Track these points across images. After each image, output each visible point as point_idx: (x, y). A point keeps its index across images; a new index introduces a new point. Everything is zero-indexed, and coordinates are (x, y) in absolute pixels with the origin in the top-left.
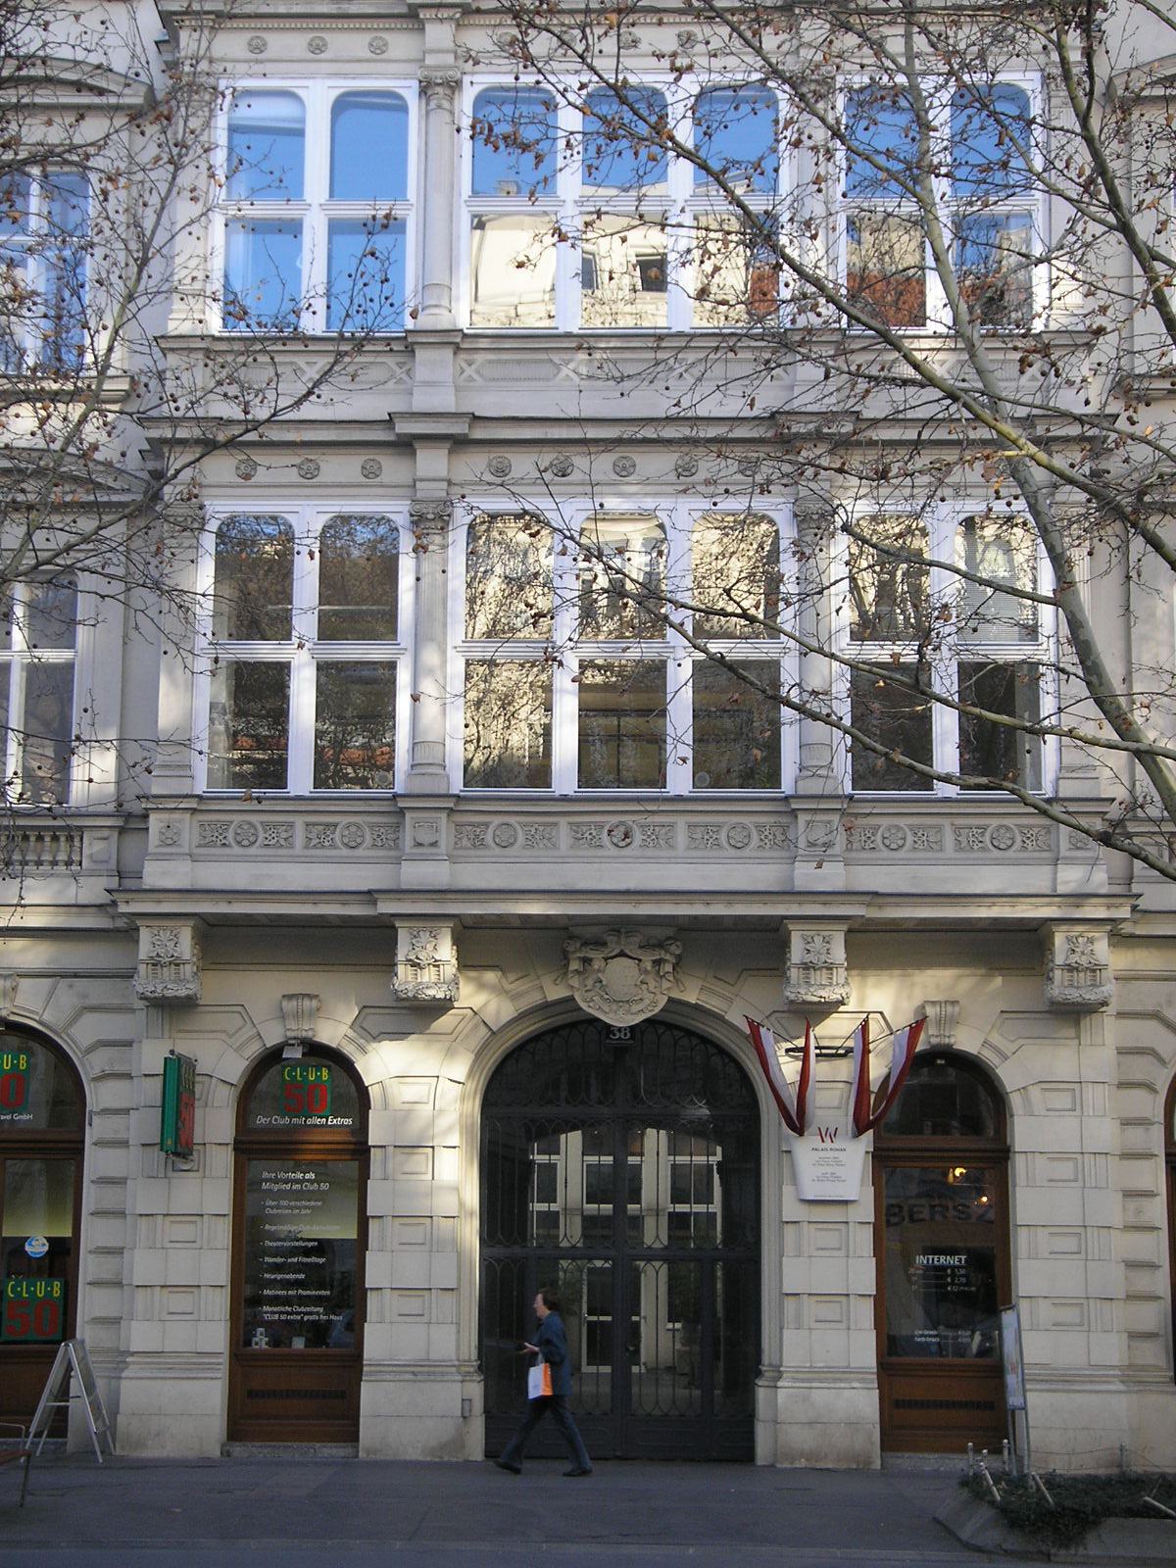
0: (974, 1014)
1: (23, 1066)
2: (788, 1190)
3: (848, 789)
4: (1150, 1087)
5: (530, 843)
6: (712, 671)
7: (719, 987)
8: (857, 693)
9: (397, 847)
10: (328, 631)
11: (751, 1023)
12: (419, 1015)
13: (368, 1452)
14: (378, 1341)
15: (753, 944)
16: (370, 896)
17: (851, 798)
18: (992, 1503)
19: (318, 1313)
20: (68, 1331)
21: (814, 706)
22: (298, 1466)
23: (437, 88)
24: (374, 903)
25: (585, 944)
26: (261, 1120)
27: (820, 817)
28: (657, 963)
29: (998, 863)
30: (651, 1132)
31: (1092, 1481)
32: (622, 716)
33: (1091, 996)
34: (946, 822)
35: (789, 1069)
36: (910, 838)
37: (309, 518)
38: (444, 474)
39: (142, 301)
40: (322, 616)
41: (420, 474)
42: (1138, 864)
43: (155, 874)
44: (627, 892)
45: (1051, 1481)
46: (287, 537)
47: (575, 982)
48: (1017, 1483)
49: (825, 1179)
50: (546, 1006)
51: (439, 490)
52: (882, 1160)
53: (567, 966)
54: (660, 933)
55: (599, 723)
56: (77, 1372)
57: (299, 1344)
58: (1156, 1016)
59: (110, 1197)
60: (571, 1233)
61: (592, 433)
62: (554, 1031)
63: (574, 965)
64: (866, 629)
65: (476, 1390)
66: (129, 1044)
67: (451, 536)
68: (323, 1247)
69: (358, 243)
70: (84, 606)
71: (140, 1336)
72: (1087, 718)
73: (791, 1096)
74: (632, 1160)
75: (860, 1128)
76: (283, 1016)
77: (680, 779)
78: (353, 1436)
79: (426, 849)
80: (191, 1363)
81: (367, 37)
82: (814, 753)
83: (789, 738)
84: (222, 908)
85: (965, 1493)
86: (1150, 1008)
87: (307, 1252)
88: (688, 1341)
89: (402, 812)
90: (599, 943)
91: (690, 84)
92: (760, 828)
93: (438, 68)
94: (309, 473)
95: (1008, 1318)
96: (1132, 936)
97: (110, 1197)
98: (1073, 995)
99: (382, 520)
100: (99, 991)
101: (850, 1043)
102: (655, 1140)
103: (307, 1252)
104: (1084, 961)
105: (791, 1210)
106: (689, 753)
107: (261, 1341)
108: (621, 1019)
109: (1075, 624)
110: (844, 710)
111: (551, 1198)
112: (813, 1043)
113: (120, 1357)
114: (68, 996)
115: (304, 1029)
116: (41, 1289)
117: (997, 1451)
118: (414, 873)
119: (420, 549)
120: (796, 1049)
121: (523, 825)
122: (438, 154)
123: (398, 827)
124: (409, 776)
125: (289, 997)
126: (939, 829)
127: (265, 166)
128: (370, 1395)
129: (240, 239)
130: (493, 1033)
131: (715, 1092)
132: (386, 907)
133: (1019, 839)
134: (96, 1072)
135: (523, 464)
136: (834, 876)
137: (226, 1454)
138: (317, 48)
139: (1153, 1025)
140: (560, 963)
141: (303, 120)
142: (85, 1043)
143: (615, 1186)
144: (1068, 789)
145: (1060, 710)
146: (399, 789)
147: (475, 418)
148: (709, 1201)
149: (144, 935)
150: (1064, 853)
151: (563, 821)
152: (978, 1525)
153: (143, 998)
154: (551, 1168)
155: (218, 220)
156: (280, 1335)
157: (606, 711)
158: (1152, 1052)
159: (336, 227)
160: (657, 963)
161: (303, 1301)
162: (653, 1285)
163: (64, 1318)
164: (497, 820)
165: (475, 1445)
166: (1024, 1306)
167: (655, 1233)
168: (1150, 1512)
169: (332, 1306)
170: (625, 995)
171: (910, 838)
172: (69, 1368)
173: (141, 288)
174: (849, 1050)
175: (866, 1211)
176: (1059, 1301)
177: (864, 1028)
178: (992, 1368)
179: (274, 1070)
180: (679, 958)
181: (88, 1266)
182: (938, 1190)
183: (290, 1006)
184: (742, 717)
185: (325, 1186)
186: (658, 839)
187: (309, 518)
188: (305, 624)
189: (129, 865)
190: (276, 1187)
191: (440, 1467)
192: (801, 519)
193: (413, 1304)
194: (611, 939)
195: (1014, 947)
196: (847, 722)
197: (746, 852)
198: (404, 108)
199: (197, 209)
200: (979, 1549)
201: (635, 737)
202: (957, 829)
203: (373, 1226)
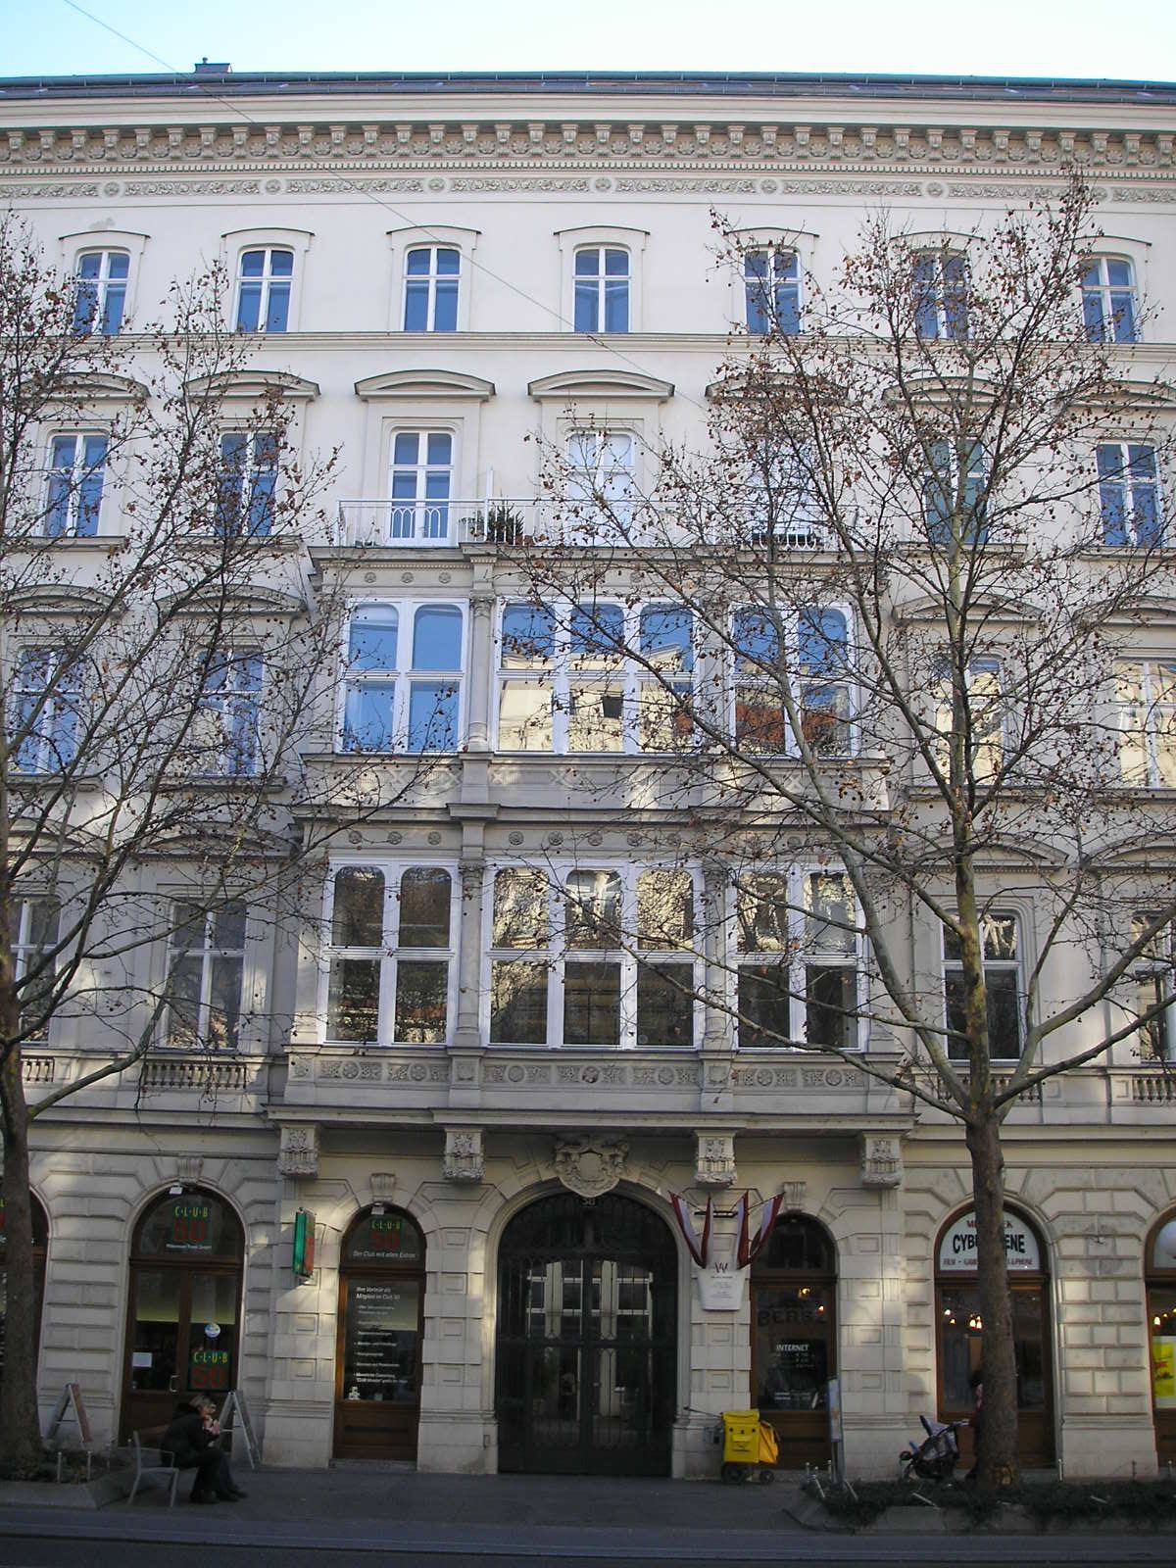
0: (815, 1191)
1: (205, 1215)
2: (695, 1304)
3: (736, 1047)
4: (926, 1237)
5: (531, 1080)
6: (649, 973)
7: (654, 1173)
8: (742, 990)
9: (447, 1080)
10: (405, 940)
11: (672, 1196)
12: (464, 1187)
13: (423, 1466)
14: (428, 1397)
15: (674, 1145)
16: (429, 1112)
17: (737, 1052)
18: (820, 1499)
19: (389, 1379)
20: (231, 1384)
21: (715, 1000)
22: (379, 1475)
23: (480, 604)
24: (432, 1116)
25: (567, 1144)
26: (357, 1254)
27: (717, 1064)
28: (613, 1157)
29: (829, 1094)
30: (607, 1264)
31: (883, 1484)
32: (592, 992)
33: (888, 1179)
34: (798, 1068)
35: (696, 1225)
36: (775, 1078)
37: (393, 870)
38: (480, 842)
39: (296, 736)
40: (401, 932)
41: (465, 842)
42: (918, 1099)
43: (291, 1094)
44: (595, 1111)
45: (858, 1486)
46: (380, 876)
47: (560, 1168)
48: (836, 1488)
49: (720, 1295)
50: (540, 1184)
51: (477, 852)
52: (755, 1284)
53: (554, 1158)
54: (614, 1137)
55: (573, 997)
56: (238, 1411)
57: (378, 1398)
58: (929, 1191)
59: (260, 1301)
60: (552, 1329)
61: (574, 818)
62: (546, 1199)
63: (559, 1158)
64: (748, 944)
65: (492, 1430)
66: (273, 1203)
67: (484, 890)
68: (394, 1336)
69: (430, 697)
70: (251, 927)
71: (278, 1390)
72: (886, 1005)
73: (698, 1243)
74: (595, 1280)
75: (741, 1266)
76: (371, 1187)
77: (628, 1042)
78: (414, 1457)
79: (465, 1082)
80: (310, 1408)
81: (438, 573)
82: (715, 1025)
83: (699, 1019)
84: (334, 1117)
85: (804, 1494)
86: (925, 1185)
87: (385, 1339)
88: (629, 1399)
89: (450, 1058)
90: (577, 1144)
91: (638, 608)
92: (680, 1071)
93: (482, 591)
94: (394, 840)
95: (833, 1384)
96: (915, 1140)
97: (260, 1301)
98: (877, 1178)
99: (441, 871)
100: (256, 1169)
101: (736, 1209)
102: (608, 1268)
103: (385, 1339)
104: (884, 1156)
105: (697, 1316)
106: (634, 1030)
107: (354, 1395)
108: (589, 1192)
109: (877, 946)
110: (733, 1002)
111: (539, 1303)
112: (712, 1209)
113: (265, 1403)
114: (235, 1170)
115: (387, 1196)
116: (215, 1357)
117: (823, 1467)
118: (457, 1098)
119: (467, 896)
120: (702, 1213)
121: (528, 1067)
122: (479, 638)
123: (448, 1067)
124: (455, 1035)
125: (377, 1175)
126: (794, 1072)
127: (376, 655)
128: (425, 1432)
129: (355, 693)
130: (507, 1201)
131: (649, 1241)
132: (439, 1119)
133: (844, 1078)
134: (252, 1220)
135: (534, 838)
136: (728, 1102)
137: (332, 1465)
138: (407, 579)
139: (928, 1197)
140: (551, 1156)
141: (397, 622)
142: (245, 1200)
143: (584, 1296)
144: (875, 1047)
145: (868, 1001)
146: (448, 1042)
147: (502, 807)
148: (645, 1308)
149: (285, 1134)
150: (872, 1087)
151: (553, 1065)
152: (810, 1513)
153: (283, 1174)
154: (540, 1286)
155: (342, 685)
156: (366, 1391)
157: (580, 991)
158: (926, 1214)
159: (415, 687)
160: (613, 1157)
161: (382, 1370)
162: (608, 1361)
163: (229, 1375)
164: (512, 1064)
165: (492, 1467)
166: (844, 1377)
167: (608, 1330)
168: (915, 1502)
169: (399, 1373)
170: (592, 1178)
171: (775, 1078)
172: (233, 1408)
173: (296, 728)
174: (736, 1214)
175: (745, 1316)
176: (866, 1374)
177: (745, 1199)
178: (823, 1415)
179: (365, 1224)
180: (627, 1154)
181: (245, 1344)
182: (791, 1302)
183: (376, 1181)
184: (669, 1002)
185: (397, 1297)
186: (614, 1077)
187: (393, 870)
188: (391, 940)
189: (275, 1088)
190: (365, 1297)
191: (469, 1478)
192: (707, 874)
193: (453, 1375)
194: (584, 1141)
195: (839, 1146)
196: (735, 1009)
197: (670, 1086)
198: (460, 615)
199: (331, 681)
200: (811, 1528)
201: (600, 1008)
202: (805, 1072)
203: (428, 1324)
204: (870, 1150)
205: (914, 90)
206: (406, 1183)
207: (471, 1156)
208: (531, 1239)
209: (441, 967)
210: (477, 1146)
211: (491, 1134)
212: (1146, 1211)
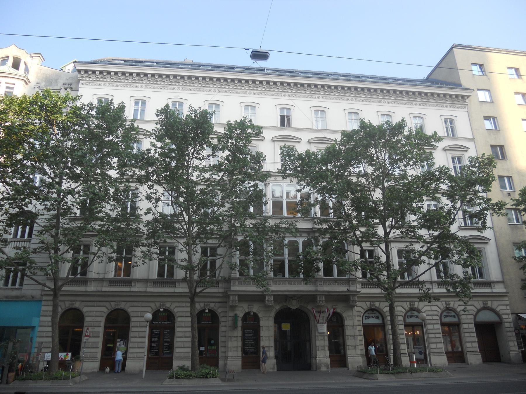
116: (213, 347)
139: (105, 308)
142: (220, 312)
170: (294, 305)
204: (318, 299)
205: (395, 81)
206: (256, 308)
207: (271, 301)
208: (279, 319)
209: (399, 259)
210: (272, 298)
211: (239, 296)
212: (439, 310)
